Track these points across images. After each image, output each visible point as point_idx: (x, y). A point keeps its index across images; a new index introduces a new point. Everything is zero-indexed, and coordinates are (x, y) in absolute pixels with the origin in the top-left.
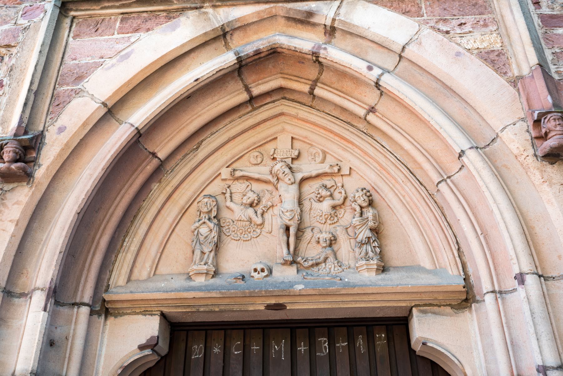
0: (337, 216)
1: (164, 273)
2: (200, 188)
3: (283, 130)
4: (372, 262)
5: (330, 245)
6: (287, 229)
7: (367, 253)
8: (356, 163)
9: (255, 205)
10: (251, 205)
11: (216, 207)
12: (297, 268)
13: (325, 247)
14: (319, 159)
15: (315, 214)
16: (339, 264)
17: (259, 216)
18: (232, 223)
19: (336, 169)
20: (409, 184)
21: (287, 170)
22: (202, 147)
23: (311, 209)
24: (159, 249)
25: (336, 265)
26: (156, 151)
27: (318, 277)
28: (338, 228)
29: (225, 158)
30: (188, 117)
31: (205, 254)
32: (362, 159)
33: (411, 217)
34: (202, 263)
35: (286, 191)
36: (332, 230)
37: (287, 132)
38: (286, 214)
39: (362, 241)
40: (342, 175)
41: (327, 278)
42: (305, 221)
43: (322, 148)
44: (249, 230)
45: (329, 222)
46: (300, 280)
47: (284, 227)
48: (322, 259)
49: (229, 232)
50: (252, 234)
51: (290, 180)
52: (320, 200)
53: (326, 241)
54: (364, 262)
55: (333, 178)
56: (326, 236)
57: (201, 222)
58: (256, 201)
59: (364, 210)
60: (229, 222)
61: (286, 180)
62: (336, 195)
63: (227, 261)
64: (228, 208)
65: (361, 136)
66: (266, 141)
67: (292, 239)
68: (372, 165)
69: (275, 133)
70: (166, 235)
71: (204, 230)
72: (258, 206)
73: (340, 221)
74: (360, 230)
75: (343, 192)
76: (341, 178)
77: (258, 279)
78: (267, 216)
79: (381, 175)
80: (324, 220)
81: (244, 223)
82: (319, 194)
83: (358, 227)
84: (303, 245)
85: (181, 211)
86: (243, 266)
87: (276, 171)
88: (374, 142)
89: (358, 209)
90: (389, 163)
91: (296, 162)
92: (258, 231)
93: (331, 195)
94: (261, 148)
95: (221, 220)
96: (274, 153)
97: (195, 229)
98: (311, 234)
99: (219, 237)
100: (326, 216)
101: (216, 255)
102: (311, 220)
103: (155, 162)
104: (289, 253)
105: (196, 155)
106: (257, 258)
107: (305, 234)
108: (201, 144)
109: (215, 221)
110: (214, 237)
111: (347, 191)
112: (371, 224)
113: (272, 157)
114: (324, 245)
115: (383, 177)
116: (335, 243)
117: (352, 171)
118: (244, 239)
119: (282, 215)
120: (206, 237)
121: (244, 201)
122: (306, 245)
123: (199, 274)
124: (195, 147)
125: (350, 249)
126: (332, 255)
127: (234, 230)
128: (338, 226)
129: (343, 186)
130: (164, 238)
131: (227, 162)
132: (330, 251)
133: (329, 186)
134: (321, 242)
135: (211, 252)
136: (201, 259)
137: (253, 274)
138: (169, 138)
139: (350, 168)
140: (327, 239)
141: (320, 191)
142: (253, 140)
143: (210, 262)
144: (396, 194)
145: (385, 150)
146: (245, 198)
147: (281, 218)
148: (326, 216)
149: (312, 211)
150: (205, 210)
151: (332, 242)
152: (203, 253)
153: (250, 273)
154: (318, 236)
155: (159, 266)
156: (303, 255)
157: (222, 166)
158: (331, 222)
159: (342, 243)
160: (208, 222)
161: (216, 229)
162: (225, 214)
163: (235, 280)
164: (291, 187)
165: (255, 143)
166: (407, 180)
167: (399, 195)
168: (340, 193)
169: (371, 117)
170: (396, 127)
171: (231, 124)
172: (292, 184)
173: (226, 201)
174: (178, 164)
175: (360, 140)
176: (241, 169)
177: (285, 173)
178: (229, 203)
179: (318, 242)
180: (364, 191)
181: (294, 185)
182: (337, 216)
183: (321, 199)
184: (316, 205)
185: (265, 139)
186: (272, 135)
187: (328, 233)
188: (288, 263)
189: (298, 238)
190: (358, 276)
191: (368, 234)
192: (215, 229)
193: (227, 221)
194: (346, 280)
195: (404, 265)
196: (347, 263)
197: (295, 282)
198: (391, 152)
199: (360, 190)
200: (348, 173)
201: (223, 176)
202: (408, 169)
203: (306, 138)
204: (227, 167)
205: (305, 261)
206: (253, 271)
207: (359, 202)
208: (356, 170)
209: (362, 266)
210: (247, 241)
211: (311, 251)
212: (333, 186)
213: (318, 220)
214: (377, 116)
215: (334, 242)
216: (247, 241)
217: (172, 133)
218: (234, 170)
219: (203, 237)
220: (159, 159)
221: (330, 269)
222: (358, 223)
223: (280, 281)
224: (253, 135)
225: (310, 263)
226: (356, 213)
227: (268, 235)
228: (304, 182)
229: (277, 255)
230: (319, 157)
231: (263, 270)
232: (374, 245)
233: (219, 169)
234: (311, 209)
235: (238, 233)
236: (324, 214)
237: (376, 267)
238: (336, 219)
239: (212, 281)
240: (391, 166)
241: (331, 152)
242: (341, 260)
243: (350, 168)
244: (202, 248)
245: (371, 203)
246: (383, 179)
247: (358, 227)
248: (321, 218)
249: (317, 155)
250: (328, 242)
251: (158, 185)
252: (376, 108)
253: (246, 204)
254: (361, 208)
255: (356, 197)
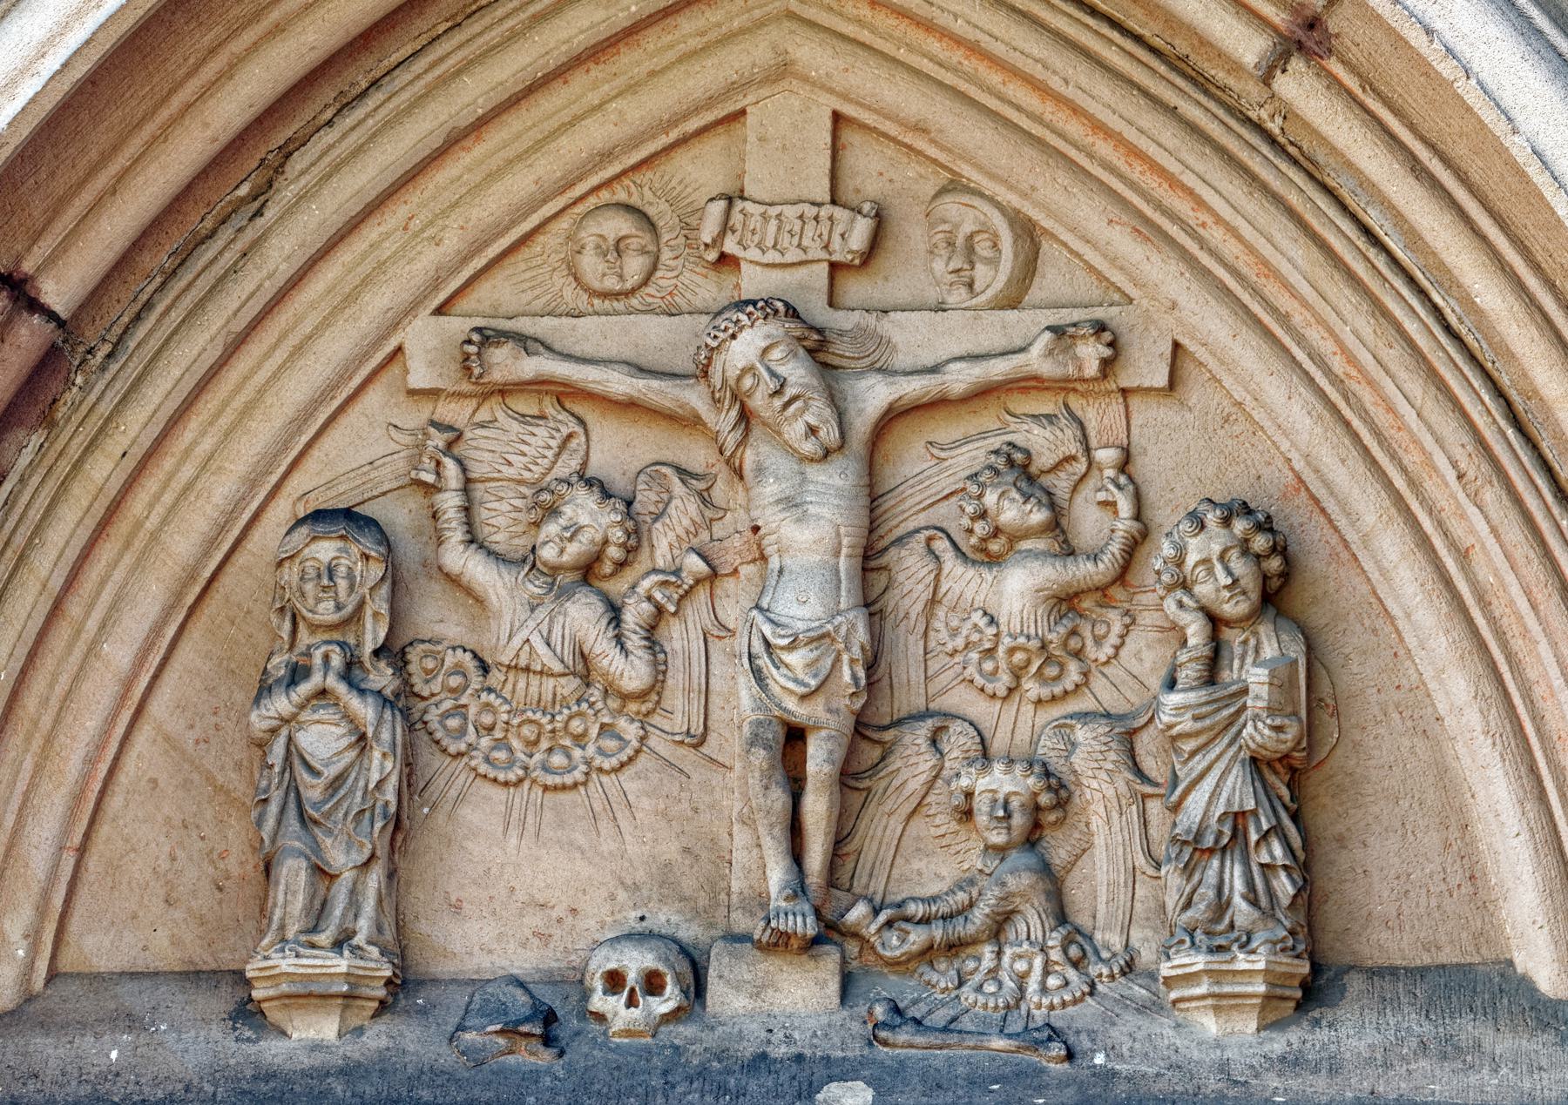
0: (1078, 654)
1: (103, 964)
2: (286, 447)
3: (782, 71)
4: (1242, 962)
5: (1032, 839)
6: (795, 736)
7: (1221, 906)
8: (1211, 326)
9: (608, 568)
10: (587, 571)
11: (385, 590)
12: (844, 962)
13: (1001, 851)
14: (993, 279)
15: (954, 633)
16: (1074, 951)
17: (635, 641)
18: (476, 681)
19: (1090, 353)
20: (1492, 495)
21: (797, 373)
22: (287, 192)
23: (934, 601)
24: (66, 831)
25: (1055, 955)
26: (28, 266)
27: (953, 1039)
28: (1081, 734)
29: (427, 259)
30: (208, 39)
31: (333, 877)
32: (1246, 297)
33: (1488, 689)
34: (324, 938)
35: (790, 503)
36: (1048, 748)
37: (805, 79)
38: (789, 658)
39: (1199, 836)
40: (1124, 392)
41: (999, 1043)
42: (900, 675)
43: (1014, 200)
44: (576, 726)
45: (1032, 688)
46: (856, 1050)
47: (776, 734)
48: (979, 916)
49: (462, 731)
50: (591, 750)
51: (812, 431)
52: (991, 550)
53: (1008, 816)
54: (1199, 961)
55: (1075, 403)
56: (1008, 788)
57: (305, 688)
58: (614, 552)
59: (1234, 638)
60: (459, 670)
61: (794, 431)
62: (1088, 521)
63: (457, 908)
64: (454, 581)
65: (1244, 155)
66: (674, 135)
67: (816, 807)
68: (1300, 340)
69: (731, 89)
70: (100, 747)
71: (322, 740)
72: (629, 575)
73: (1098, 683)
74: (1199, 764)
75: (1125, 507)
76: (1116, 407)
77: (628, 1033)
78: (681, 637)
79: (1347, 413)
80: (1005, 679)
81: (550, 683)
82: (983, 515)
83: (1188, 746)
84: (880, 828)
85: (179, 596)
86: (544, 938)
87: (732, 374)
88: (1322, 202)
89: (1196, 631)
90: (1394, 355)
91: (856, 289)
92: (631, 731)
93: (1057, 526)
94: (646, 176)
95: (414, 655)
96: (726, 227)
97: (274, 731)
98: (925, 763)
99: (411, 779)
100: (1019, 657)
101: (391, 875)
102: (934, 666)
103: (30, 335)
104: (799, 888)
105: (257, 243)
106: (622, 895)
107: (895, 763)
108: (279, 170)
109: (382, 677)
110: (380, 784)
111: (1152, 494)
112: (1257, 734)
113: (712, 256)
114: (998, 838)
115: (1356, 423)
116: (1059, 823)
117: (1188, 367)
118: (551, 780)
119: (764, 661)
120: (340, 779)
121: (548, 553)
122: (896, 825)
123: (309, 996)
124: (244, 190)
125: (1141, 861)
126: (1039, 900)
127: (487, 719)
128: (1084, 717)
129: (1124, 465)
130: (91, 761)
131: (436, 284)
132: (1026, 880)
133: (1044, 460)
134: (982, 819)
135: (367, 864)
136: (318, 914)
137: (600, 1001)
138: (102, 180)
139: (1176, 346)
140: (1015, 803)
141: (990, 498)
142: (596, 134)
143: (364, 926)
144: (1424, 542)
145: (1381, 262)
146: (552, 529)
147: (758, 675)
148: (1019, 657)
149: (941, 612)
150: (326, 612)
151: (1051, 805)
152: (322, 873)
153: (586, 995)
154: (964, 782)
155: (75, 925)
156: (878, 886)
157: (411, 310)
158: (1045, 692)
159: (1097, 822)
160: (341, 688)
161: (389, 732)
162: (436, 617)
163: (501, 1041)
164: (817, 474)
165: (606, 156)
166: (1485, 468)
167: (1438, 542)
168: (1109, 505)
169: (1298, 87)
170: (1436, 167)
171: (459, 37)
172: (828, 453)
173: (440, 542)
174: (148, 305)
175: (1235, 189)
176: (525, 325)
177: (790, 392)
178: (457, 557)
179: (967, 814)
180: (1240, 526)
181: (838, 462)
182: (1078, 654)
183: (994, 547)
184: (962, 580)
185: (673, 123)
186: (710, 102)
187: (1018, 769)
188: (795, 943)
189: (851, 779)
190: (1163, 1029)
191: (1238, 790)
192: (386, 735)
193: (450, 660)
194: (1099, 1059)
195: (1427, 960)
196: (1116, 941)
197: (827, 1060)
198: (1411, 280)
199: (1212, 518)
200: (1161, 380)
201: (420, 377)
202: (1499, 393)
203: (920, 129)
204: (440, 311)
205: (889, 924)
206: (598, 985)
207: (1204, 590)
208: (1212, 364)
209: (1190, 978)
210: (564, 788)
211: (930, 862)
212: (1070, 459)
213: (971, 671)
214: (1334, 83)
215: (1052, 817)
216: (564, 788)
217: (116, 148)
218: (488, 338)
219: (321, 782)
220: (51, 315)
221: (1022, 978)
222: (1187, 725)
223: (748, 1050)
224: (594, 98)
225: (917, 937)
226: (1183, 657)
227: (685, 757)
228: (900, 429)
229: (736, 886)
230: (993, 262)
231: (653, 984)
232: (1265, 859)
233: (395, 326)
234: (934, 601)
235: (516, 744)
236: (1007, 641)
237: (1262, 989)
238: (1073, 668)
239: (377, 1037)
240: (1402, 375)
241: (1066, 236)
242: (1083, 920)
243: (1176, 346)
244: (317, 848)
245: (1277, 594)
246: (1355, 437)
247: (1188, 746)
248: (988, 666)
249: (983, 249)
250: (1018, 820)
251: (36, 439)
252: (1333, 24)
253: (555, 570)
254: (1215, 622)
255: (1192, 558)
